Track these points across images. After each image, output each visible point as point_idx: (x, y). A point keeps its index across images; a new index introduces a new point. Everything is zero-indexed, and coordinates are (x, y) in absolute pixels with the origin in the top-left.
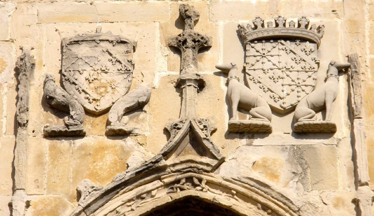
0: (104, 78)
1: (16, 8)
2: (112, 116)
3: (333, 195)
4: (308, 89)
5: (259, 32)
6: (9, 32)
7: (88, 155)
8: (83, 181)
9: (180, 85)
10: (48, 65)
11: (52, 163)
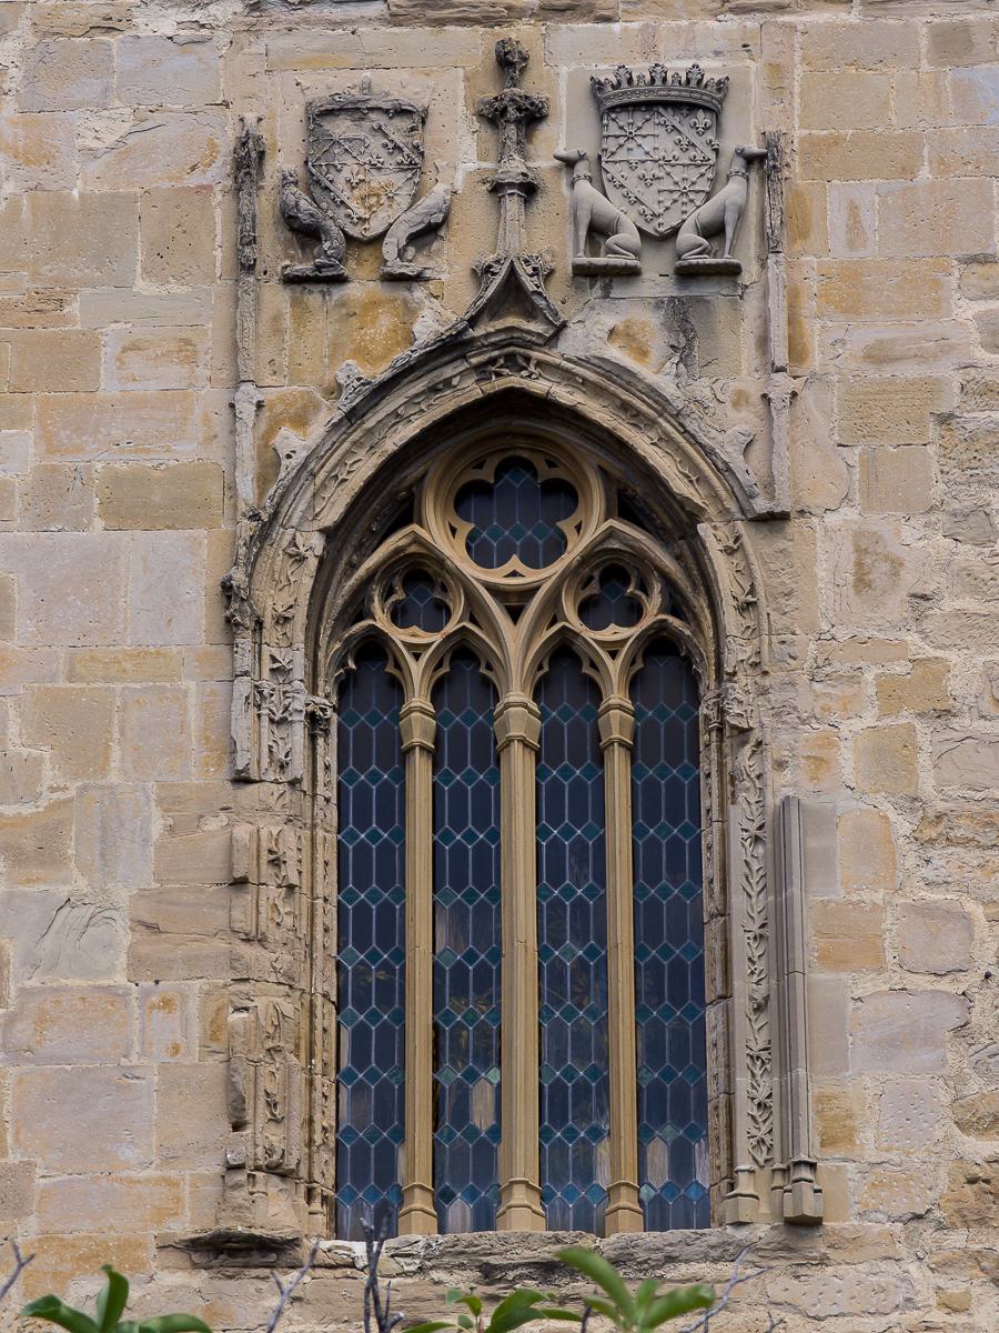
0: (377, 179)
1: (231, 42)
2: (389, 249)
3: (734, 386)
4: (699, 199)
5: (623, 93)
6: (221, 88)
7: (352, 316)
8: (345, 363)
9: (497, 189)
10: (285, 159)
11: (296, 331)
